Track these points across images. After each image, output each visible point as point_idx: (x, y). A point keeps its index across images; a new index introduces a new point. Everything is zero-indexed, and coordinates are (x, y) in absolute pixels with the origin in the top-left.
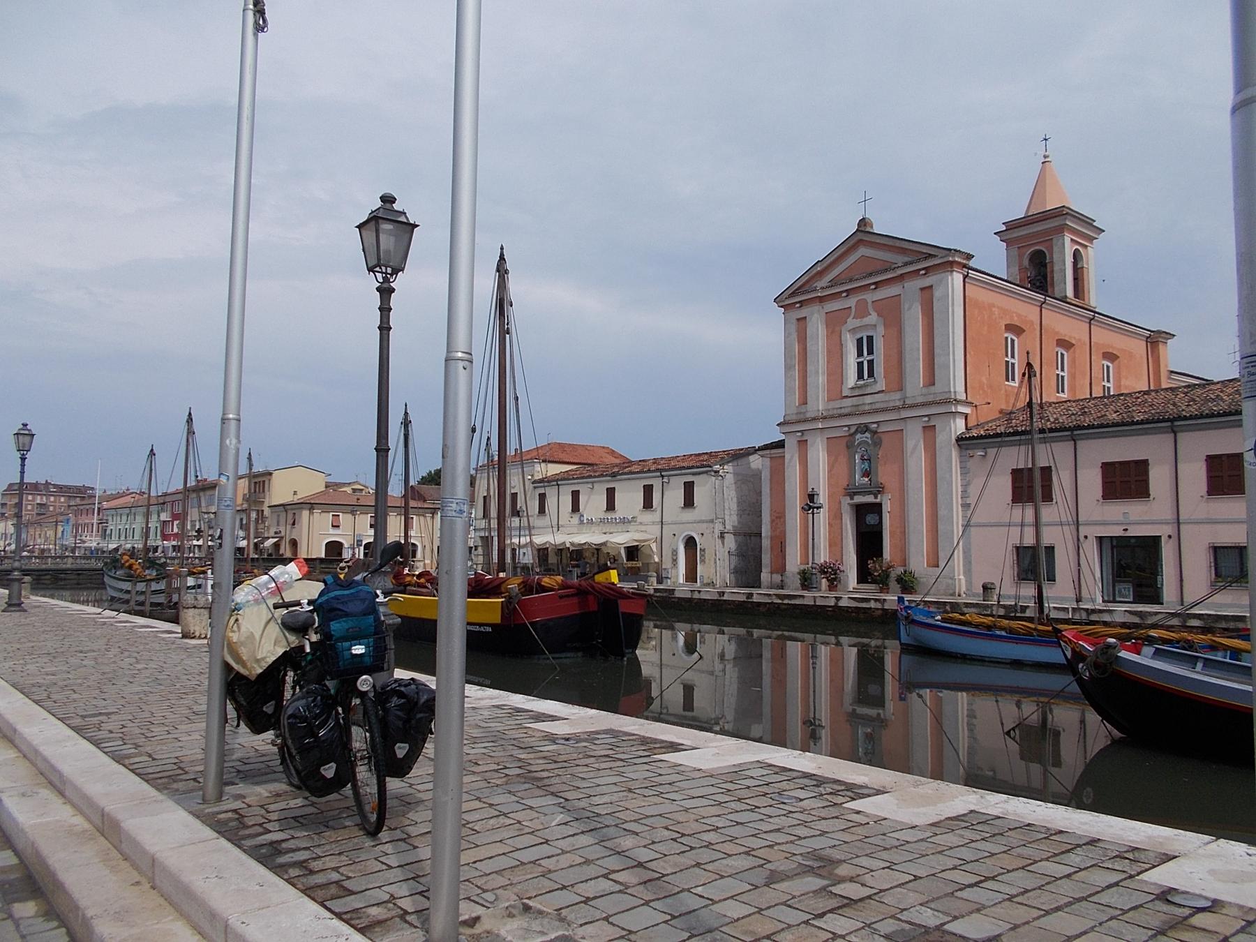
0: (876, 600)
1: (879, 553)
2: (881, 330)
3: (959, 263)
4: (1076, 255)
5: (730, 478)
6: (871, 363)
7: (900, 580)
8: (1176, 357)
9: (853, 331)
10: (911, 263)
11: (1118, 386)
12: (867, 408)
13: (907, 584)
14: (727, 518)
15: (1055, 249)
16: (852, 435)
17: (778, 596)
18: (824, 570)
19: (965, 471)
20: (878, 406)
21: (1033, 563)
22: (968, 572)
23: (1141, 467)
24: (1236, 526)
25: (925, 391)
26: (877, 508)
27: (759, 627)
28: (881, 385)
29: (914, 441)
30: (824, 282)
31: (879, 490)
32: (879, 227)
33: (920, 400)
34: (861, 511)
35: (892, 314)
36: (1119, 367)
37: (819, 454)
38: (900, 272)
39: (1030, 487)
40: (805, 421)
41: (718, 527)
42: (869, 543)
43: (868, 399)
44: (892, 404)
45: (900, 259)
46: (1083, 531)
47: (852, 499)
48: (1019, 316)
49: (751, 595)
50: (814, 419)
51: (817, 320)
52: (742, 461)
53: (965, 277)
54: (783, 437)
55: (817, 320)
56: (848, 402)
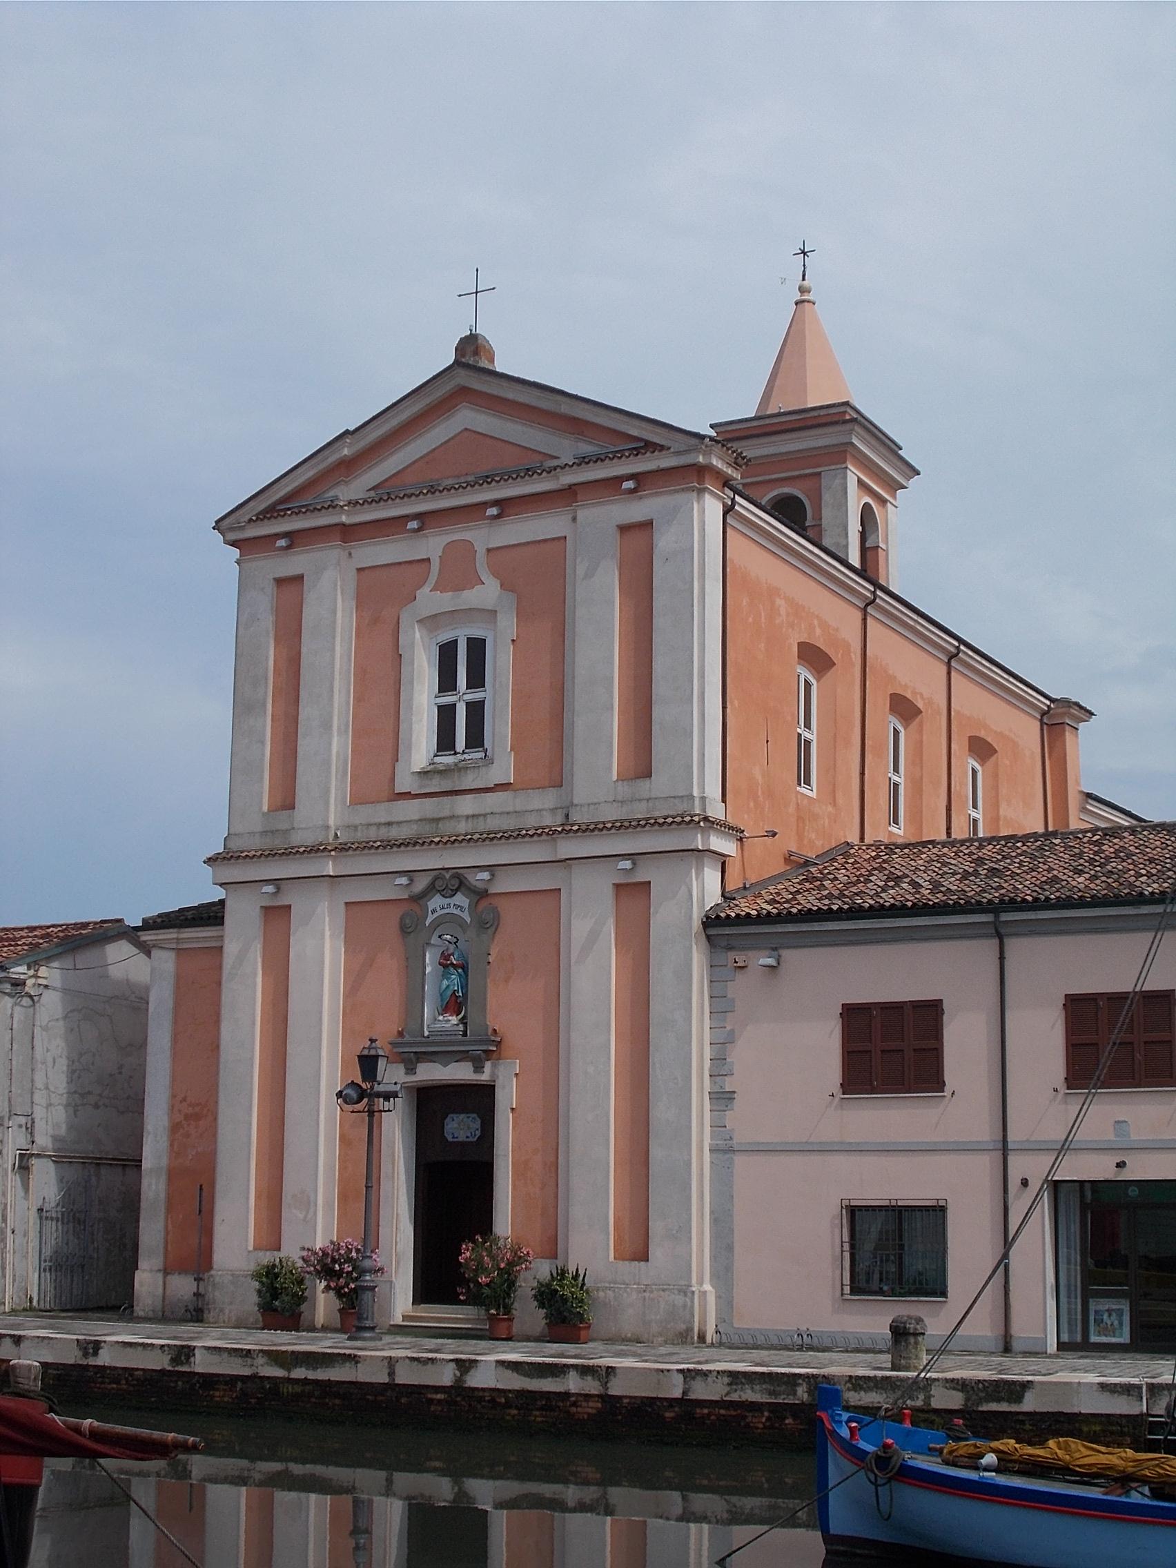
0: (585, 1371)
1: (485, 1225)
2: (508, 625)
3: (718, 473)
4: (867, 515)
5: (52, 1004)
6: (476, 711)
7: (547, 1296)
8: (1096, 760)
9: (431, 622)
10: (599, 459)
11: (994, 820)
12: (462, 827)
13: (565, 1311)
14: (39, 1113)
15: (827, 497)
16: (419, 899)
17: (275, 1357)
18: (329, 1266)
19: (721, 1006)
20: (493, 824)
21: (893, 1250)
22: (723, 1274)
23: (927, 1016)
24: (783, 1159)
25: (624, 790)
26: (480, 1099)
27: (211, 1449)
28: (503, 768)
29: (590, 919)
30: (357, 487)
31: (487, 1049)
32: (509, 359)
33: (610, 814)
34: (431, 1104)
35: (541, 588)
36: (996, 776)
37: (322, 946)
38: (567, 479)
39: (891, 1051)
40: (289, 853)
41: (15, 1140)
42: (454, 1191)
43: (466, 805)
44: (531, 821)
45: (565, 448)
46: (1019, 1166)
47: (411, 1070)
48: (824, 625)
49: (94, 1347)
50: (314, 850)
51: (331, 585)
52: (86, 958)
53: (728, 510)
54: (218, 894)
55: (331, 585)
56: (411, 810)
